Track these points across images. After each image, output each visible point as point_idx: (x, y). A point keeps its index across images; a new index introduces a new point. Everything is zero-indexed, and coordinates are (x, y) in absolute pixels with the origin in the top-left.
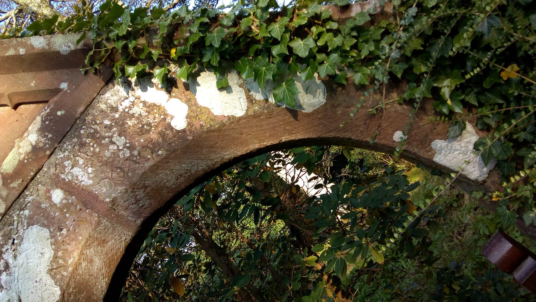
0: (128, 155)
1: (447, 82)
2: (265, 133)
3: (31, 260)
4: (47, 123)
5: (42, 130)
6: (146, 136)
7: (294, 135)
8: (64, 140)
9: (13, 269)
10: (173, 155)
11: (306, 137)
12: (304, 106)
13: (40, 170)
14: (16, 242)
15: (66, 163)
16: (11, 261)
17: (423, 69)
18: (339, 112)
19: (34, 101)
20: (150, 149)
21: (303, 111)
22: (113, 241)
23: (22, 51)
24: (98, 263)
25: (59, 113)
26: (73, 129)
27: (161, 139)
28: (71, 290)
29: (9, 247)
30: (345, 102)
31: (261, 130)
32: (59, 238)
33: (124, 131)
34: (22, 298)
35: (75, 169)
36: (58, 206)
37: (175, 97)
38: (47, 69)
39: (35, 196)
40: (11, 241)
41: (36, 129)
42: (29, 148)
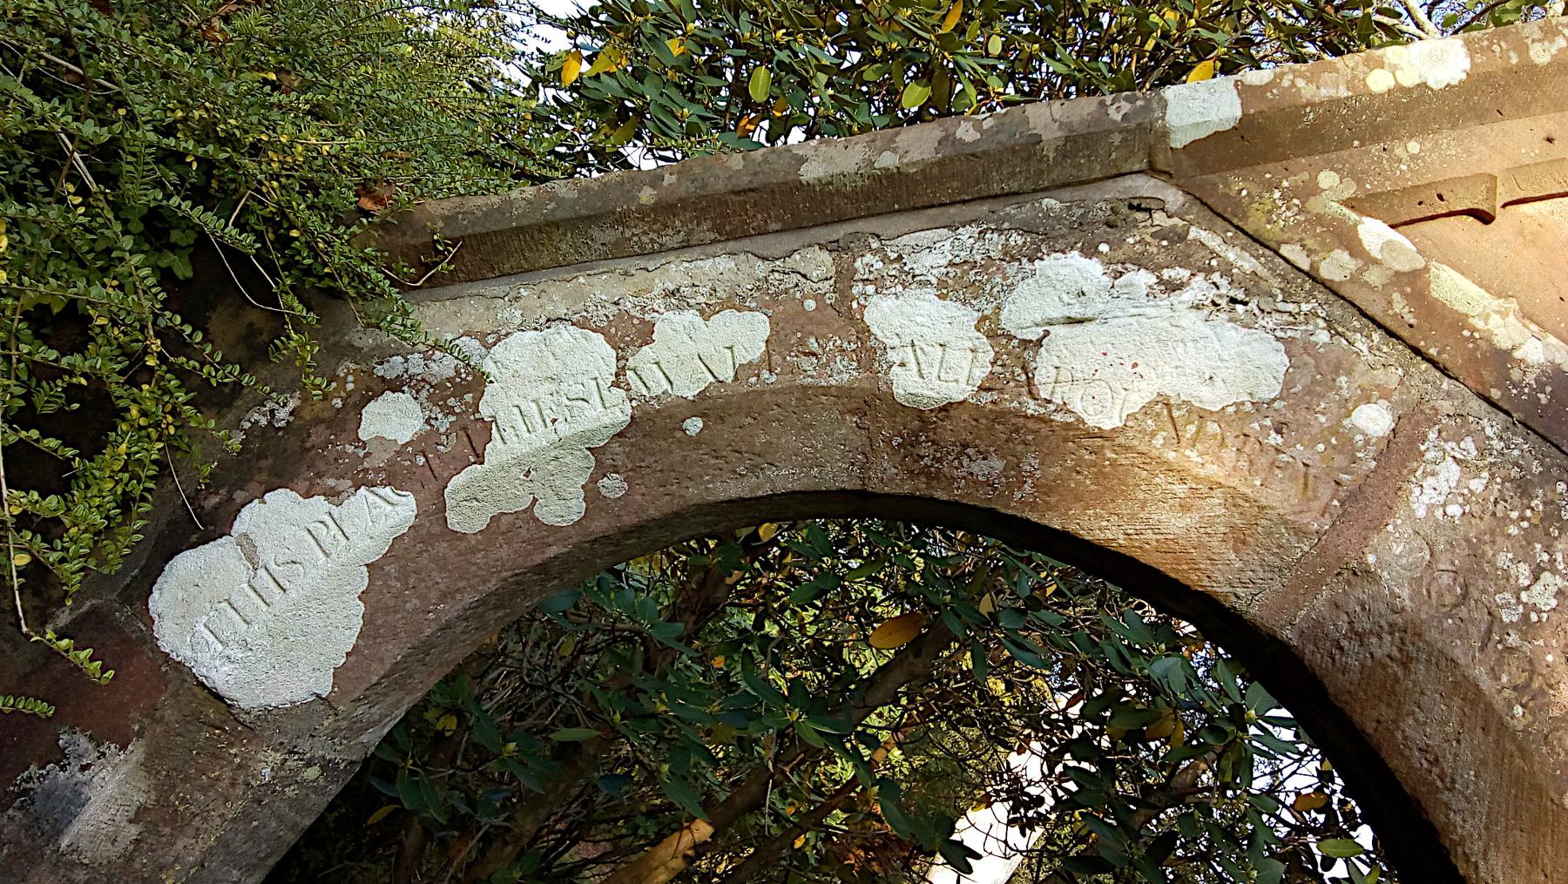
0: (1506, 620)
3: (1192, 351)
8: (1533, 436)
10: (1510, 747)
13: (1444, 371)
14: (1239, 307)
15: (1469, 444)
16: (1187, 296)
22: (1238, 565)
24: (1176, 523)
28: (1109, 455)
29: (1223, 291)
32: (1256, 426)
34: (1089, 326)
35: (1455, 468)
36: (1346, 422)
40: (1241, 296)
41: (1558, 361)
42: (1503, 343)
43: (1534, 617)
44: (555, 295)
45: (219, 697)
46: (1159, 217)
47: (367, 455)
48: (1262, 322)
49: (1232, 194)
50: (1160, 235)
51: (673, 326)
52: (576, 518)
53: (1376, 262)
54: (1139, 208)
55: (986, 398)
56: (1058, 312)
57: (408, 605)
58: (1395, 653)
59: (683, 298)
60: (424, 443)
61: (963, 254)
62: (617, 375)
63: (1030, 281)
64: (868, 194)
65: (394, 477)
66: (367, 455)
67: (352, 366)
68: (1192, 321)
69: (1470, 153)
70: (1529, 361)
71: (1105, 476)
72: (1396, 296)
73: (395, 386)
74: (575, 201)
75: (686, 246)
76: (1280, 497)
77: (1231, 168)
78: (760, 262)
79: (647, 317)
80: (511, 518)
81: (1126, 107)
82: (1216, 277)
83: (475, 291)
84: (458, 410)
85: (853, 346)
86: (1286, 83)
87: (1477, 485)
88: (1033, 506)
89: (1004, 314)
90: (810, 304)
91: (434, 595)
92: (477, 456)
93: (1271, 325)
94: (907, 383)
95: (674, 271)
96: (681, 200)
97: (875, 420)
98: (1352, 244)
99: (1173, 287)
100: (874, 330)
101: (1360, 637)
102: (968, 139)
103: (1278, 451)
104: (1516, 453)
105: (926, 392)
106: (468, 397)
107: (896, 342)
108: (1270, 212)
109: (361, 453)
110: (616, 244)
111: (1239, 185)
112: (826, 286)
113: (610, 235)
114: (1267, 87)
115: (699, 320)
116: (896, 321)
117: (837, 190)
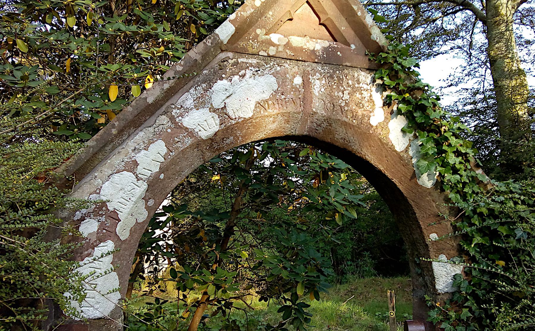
0: (343, 105)
1: (479, 238)
2: (393, 169)
3: (256, 88)
4: (330, 50)
5: (325, 50)
6: (357, 108)
7: (400, 184)
8: (327, 65)
9: (244, 80)
10: (357, 129)
11: (402, 191)
12: (420, 179)
13: (305, 61)
14: (259, 72)
15: (317, 74)
16: (247, 76)
17: (477, 223)
18: (427, 198)
19: (333, 33)
20: (353, 115)
21: (417, 180)
22: (290, 126)
23: (359, 14)
24: (273, 126)
25: (339, 53)
26: (336, 66)
27: (360, 117)
28: (254, 121)
29: (253, 70)
30: (436, 198)
31: (394, 166)
32: (278, 96)
33: (352, 95)
34: (232, 96)
35: (318, 81)
36: (293, 84)
37: (384, 110)
38: (355, 32)
39: (290, 67)
40: (258, 69)
41: (323, 46)
42: (312, 48)
43: (347, 101)
44: (106, 169)
45: (100, 319)
46: (230, 61)
47: (89, 240)
48: (265, 73)
49: (242, 47)
50: (233, 65)
51: (140, 157)
52: (147, 216)
53: (279, 45)
54: (224, 61)
55: (223, 126)
56: (224, 98)
57: (124, 264)
58: (328, 125)
59: (139, 149)
60: (102, 226)
61: (195, 96)
62: (137, 178)
63: (214, 93)
64: (165, 96)
65: (101, 240)
66: (89, 240)
67: (67, 223)
68: (251, 81)
69: (282, 8)
70: (318, 49)
71: (255, 126)
72: (287, 51)
73: (83, 219)
74: (97, 144)
75: (129, 135)
76: (291, 108)
77: (238, 41)
78: (150, 128)
79: (133, 159)
80: (134, 227)
81: (210, 41)
82: (250, 68)
83: (83, 183)
84: (104, 213)
85: (186, 134)
86: (239, 15)
87: (324, 82)
88: (243, 141)
89: (214, 105)
90: (169, 130)
91: (128, 257)
92: (118, 220)
93: (267, 72)
94: (204, 135)
95: (131, 144)
96: (124, 127)
97: (201, 146)
98: (270, 43)
99: (243, 76)
100: (188, 127)
101: (320, 125)
102: (181, 70)
103: (285, 99)
104: (326, 70)
105: (209, 134)
106: (104, 208)
107: (195, 126)
108: (252, 46)
109: (88, 241)
110: (113, 147)
111: (242, 44)
112: (170, 124)
113: (110, 146)
114: (236, 18)
115: (145, 152)
116: (191, 121)
117: (158, 100)
